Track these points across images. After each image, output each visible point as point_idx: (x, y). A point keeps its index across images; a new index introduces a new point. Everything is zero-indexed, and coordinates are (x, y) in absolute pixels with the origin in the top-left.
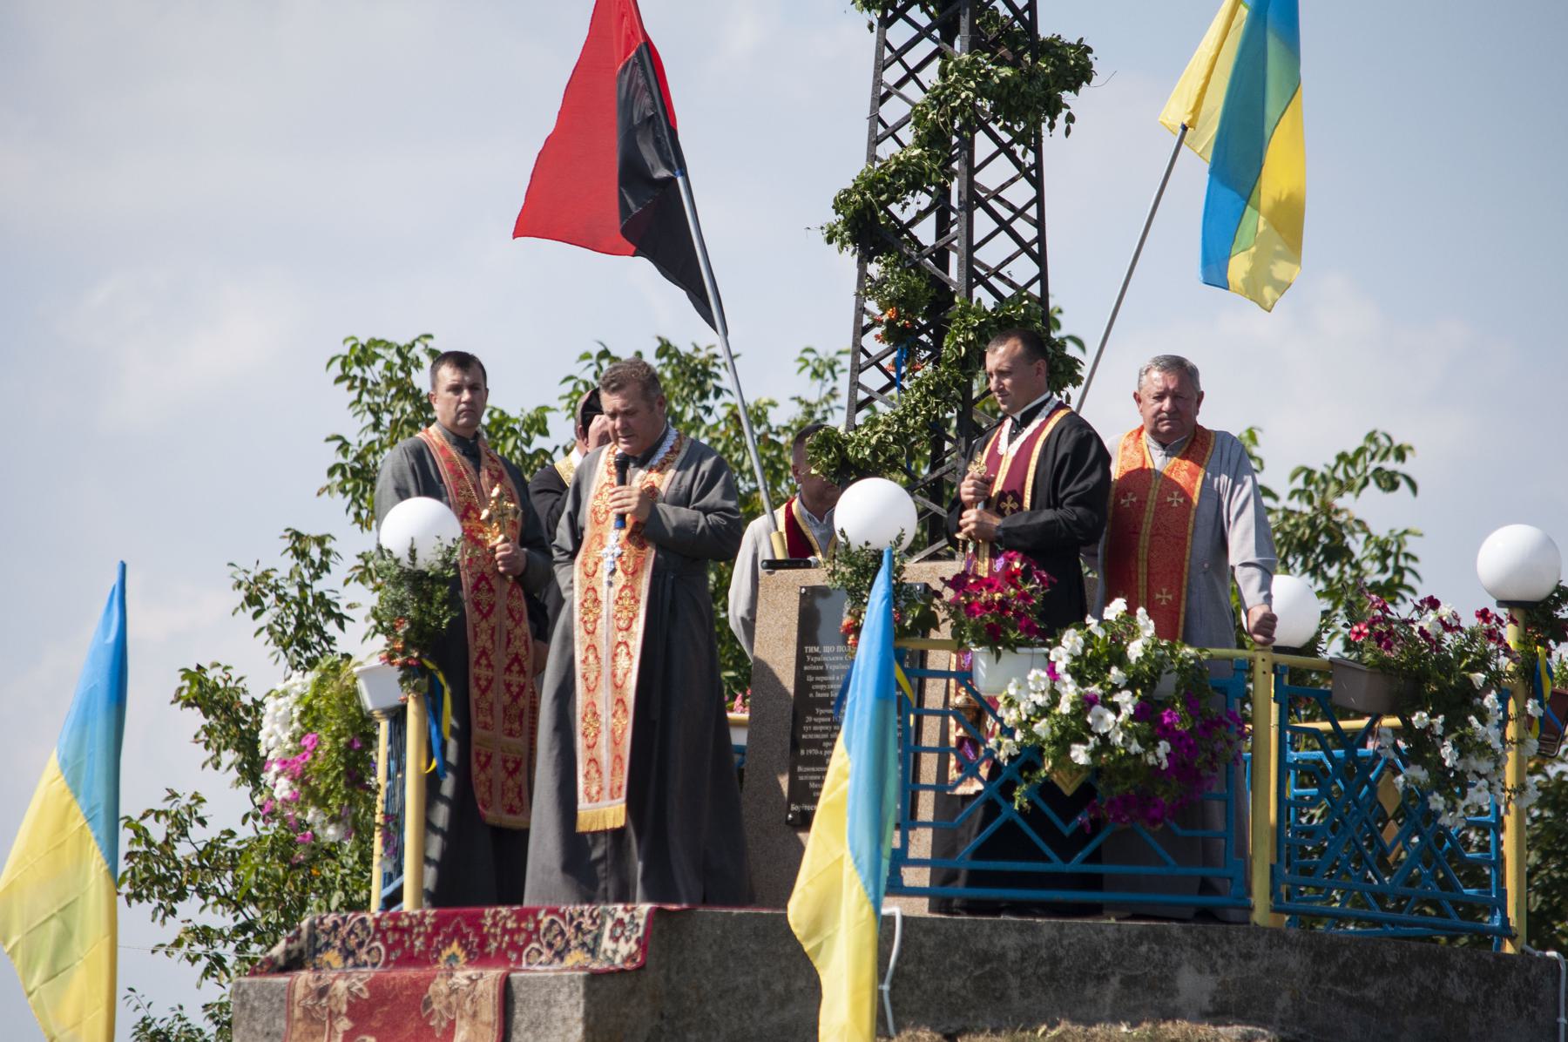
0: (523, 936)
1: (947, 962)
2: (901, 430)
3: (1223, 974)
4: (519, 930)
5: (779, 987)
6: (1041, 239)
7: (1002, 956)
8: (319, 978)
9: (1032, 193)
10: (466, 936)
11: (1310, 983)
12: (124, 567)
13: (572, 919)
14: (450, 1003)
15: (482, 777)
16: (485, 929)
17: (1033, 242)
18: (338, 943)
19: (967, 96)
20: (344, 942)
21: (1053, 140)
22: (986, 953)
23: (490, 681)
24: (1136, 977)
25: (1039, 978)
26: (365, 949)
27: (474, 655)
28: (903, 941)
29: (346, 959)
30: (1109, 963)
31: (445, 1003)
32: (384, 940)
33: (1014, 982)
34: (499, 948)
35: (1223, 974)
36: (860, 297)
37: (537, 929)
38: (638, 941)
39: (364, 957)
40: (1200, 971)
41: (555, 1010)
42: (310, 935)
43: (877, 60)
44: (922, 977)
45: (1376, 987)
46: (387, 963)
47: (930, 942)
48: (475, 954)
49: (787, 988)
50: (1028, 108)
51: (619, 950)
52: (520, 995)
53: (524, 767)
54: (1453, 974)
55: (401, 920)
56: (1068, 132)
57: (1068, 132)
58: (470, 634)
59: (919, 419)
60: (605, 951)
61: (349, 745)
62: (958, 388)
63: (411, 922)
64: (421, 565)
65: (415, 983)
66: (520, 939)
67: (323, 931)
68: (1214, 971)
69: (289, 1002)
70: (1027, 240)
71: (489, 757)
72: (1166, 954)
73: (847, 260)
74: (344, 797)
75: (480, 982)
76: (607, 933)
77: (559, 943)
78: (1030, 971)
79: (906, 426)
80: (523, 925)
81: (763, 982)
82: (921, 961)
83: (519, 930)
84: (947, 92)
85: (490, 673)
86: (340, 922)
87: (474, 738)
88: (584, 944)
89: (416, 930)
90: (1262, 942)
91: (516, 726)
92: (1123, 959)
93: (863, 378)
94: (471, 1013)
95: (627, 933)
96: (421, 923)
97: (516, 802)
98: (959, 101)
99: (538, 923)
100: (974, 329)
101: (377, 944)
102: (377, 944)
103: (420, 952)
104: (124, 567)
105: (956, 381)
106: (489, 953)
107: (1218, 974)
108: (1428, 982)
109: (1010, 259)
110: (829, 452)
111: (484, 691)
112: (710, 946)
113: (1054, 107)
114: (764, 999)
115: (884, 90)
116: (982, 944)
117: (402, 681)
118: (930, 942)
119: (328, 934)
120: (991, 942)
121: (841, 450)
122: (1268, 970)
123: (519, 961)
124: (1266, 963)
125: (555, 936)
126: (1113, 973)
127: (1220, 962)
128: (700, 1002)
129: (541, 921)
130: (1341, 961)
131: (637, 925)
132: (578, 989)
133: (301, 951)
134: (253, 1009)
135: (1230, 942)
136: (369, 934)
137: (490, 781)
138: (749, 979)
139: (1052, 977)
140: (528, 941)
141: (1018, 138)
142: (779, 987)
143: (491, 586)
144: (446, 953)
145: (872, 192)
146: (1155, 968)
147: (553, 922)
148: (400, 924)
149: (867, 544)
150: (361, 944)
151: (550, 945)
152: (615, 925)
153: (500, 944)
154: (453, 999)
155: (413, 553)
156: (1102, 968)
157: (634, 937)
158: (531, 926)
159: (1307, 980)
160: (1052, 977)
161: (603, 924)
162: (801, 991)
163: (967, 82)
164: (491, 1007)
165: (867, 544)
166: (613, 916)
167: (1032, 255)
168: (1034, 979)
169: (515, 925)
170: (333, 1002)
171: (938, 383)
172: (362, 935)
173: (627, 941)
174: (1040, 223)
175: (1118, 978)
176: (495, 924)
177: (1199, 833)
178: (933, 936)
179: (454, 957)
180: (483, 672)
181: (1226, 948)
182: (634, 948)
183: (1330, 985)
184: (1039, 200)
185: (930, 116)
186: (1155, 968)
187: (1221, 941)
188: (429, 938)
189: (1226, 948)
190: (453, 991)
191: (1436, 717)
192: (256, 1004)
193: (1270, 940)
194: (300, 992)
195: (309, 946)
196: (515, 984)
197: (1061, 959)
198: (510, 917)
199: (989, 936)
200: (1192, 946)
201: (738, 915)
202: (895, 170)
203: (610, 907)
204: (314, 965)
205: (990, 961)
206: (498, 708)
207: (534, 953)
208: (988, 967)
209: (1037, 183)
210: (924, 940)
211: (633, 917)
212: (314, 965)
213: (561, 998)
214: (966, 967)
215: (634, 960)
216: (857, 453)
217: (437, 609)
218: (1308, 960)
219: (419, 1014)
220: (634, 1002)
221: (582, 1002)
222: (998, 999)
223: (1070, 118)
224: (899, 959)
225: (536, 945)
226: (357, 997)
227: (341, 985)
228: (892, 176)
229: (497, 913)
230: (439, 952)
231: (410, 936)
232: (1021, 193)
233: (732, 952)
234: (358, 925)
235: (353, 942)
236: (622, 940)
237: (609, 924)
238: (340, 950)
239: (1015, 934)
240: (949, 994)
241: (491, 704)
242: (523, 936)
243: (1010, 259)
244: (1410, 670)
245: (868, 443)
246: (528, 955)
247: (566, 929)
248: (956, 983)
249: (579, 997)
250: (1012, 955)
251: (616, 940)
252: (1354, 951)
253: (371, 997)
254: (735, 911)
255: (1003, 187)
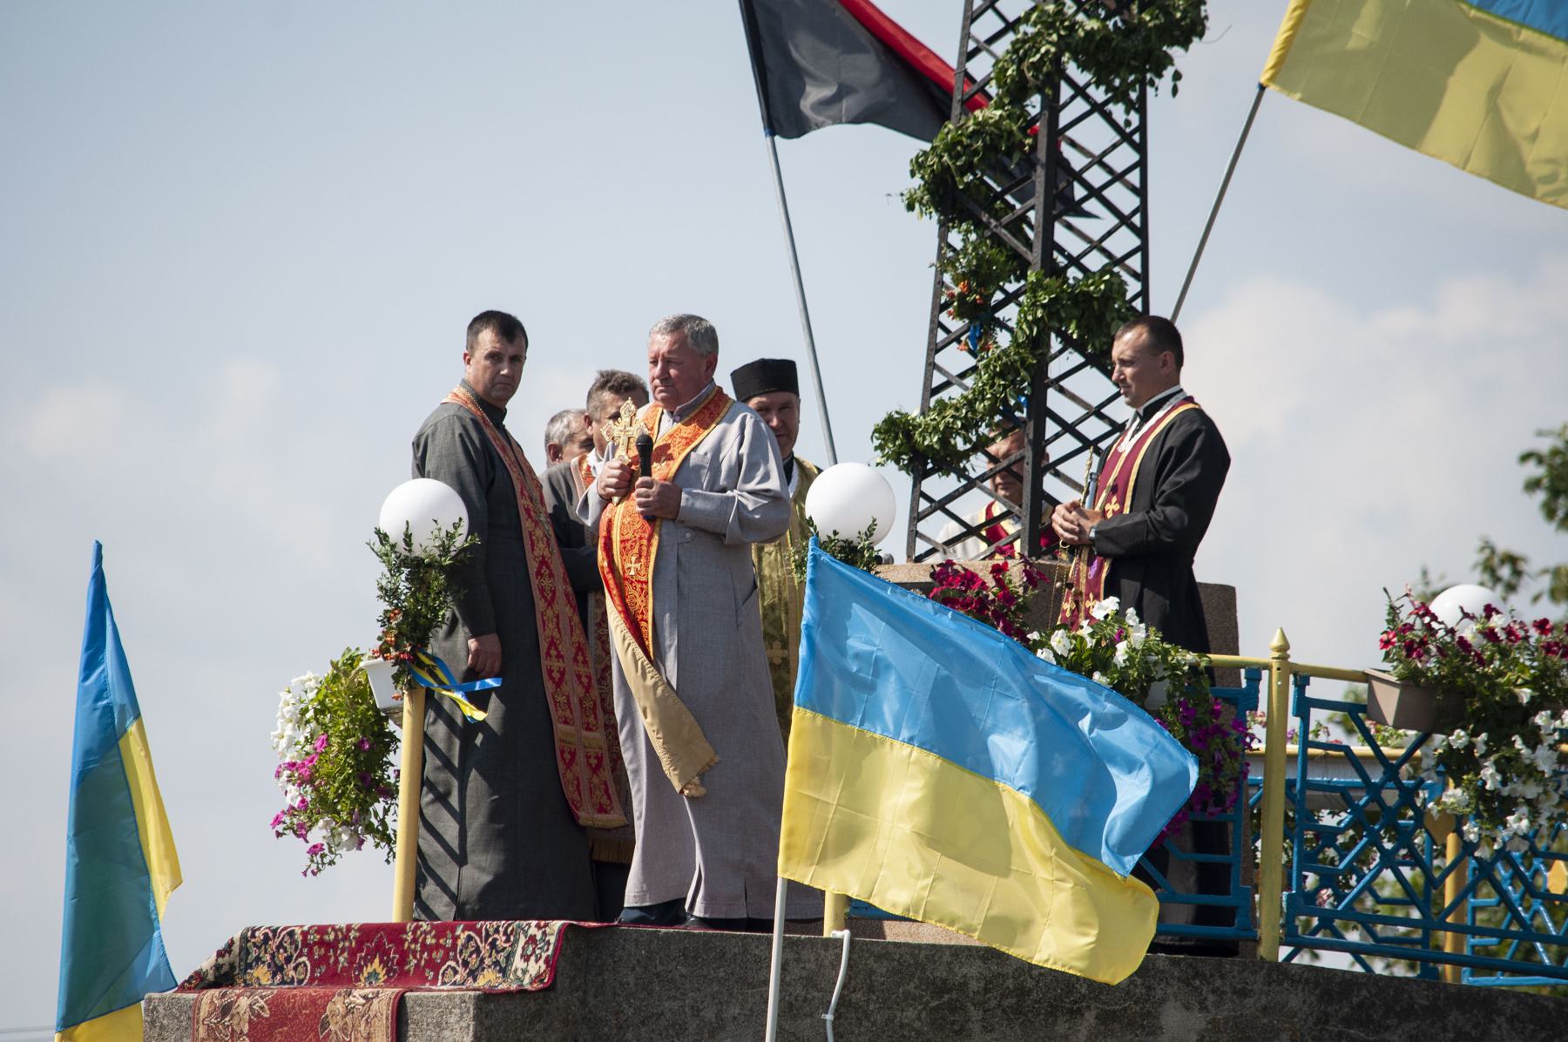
0: (441, 952)
1: (901, 990)
2: (970, 415)
3: (1213, 1012)
4: (438, 946)
5: (709, 1014)
6: (1143, 209)
7: (963, 986)
8: (224, 996)
9: (1134, 157)
10: (387, 952)
11: (1316, 1024)
12: (99, 547)
13: (488, 935)
14: (346, 1023)
15: (569, 775)
16: (406, 945)
17: (1134, 213)
18: (268, 957)
19: (1047, 52)
20: (273, 956)
21: (1158, 99)
22: (944, 981)
23: (562, 673)
24: (1114, 1012)
25: (1004, 1011)
26: (292, 965)
27: (544, 646)
28: (849, 967)
29: (274, 975)
30: (1084, 996)
31: (341, 1024)
32: (310, 955)
33: (975, 1014)
34: (417, 966)
35: (1213, 1012)
36: (941, 271)
37: (454, 945)
38: (547, 961)
39: (292, 973)
40: (1187, 1007)
41: (447, 1033)
42: (241, 948)
43: (966, 11)
44: (871, 1007)
45: (1399, 1031)
46: (312, 980)
47: (881, 969)
48: (395, 972)
49: (719, 1015)
50: (1121, 64)
51: (528, 970)
52: (414, 1015)
53: (606, 762)
54: (1501, 1020)
55: (327, 933)
56: (1175, 91)
57: (1175, 91)
58: (539, 623)
59: (987, 403)
60: (516, 970)
61: (359, 745)
62: (1027, 369)
63: (336, 936)
64: (417, 552)
65: (313, 1001)
66: (438, 956)
67: (254, 944)
68: (1203, 1008)
69: (193, 1020)
70: (1127, 212)
71: (573, 754)
72: (1149, 988)
73: (927, 224)
74: (354, 802)
75: (375, 1001)
76: (519, 951)
77: (474, 961)
78: (993, 1003)
79: (974, 411)
80: (441, 941)
81: (693, 1008)
82: (871, 989)
83: (438, 946)
84: (1027, 46)
85: (561, 664)
86: (271, 935)
87: (558, 735)
88: (496, 963)
89: (340, 946)
90: (1260, 978)
91: (591, 719)
92: (1101, 992)
93: (940, 359)
94: (365, 1035)
95: (538, 952)
96: (346, 938)
97: (604, 800)
98: (1038, 56)
99: (455, 938)
100: (1044, 306)
101: (304, 959)
102: (304, 959)
103: (343, 967)
104: (99, 547)
105: (1023, 361)
106: (409, 971)
107: (1208, 1012)
108: (1468, 1028)
109: (1110, 233)
110: (896, 438)
111: (558, 684)
112: (633, 969)
113: (1161, 63)
114: (692, 1026)
115: (972, 45)
116: (941, 973)
117: (396, 678)
118: (881, 969)
119: (259, 948)
120: (951, 970)
121: (909, 436)
122: (1265, 1008)
123: (435, 981)
124: (1264, 1001)
125: (470, 956)
126: (1088, 1007)
127: (1211, 998)
128: (620, 1028)
129: (459, 937)
130: (1355, 1000)
131: (548, 943)
132: (468, 1012)
133: (232, 966)
134: (162, 1027)
135: (1222, 977)
136: (296, 950)
137: (578, 779)
138: (675, 1005)
139: (1018, 1010)
140: (445, 959)
141: (1119, 95)
142: (709, 1014)
143: (550, 571)
144: (368, 970)
145: (950, 155)
146: (1136, 1003)
147: (470, 938)
148: (326, 937)
149: (835, 533)
150: (288, 960)
151: (465, 964)
152: (527, 943)
153: (419, 961)
154: (348, 1019)
155: (408, 538)
156: (1075, 1002)
157: (544, 955)
158: (449, 942)
159: (1311, 1020)
160: (1018, 1010)
161: (517, 941)
162: (735, 1018)
163: (1050, 35)
164: (383, 1028)
165: (835, 533)
166: (525, 933)
167: (1132, 227)
168: (999, 1012)
169: (434, 941)
170: (235, 1022)
171: (1006, 364)
172: (290, 949)
173: (537, 961)
174: (1141, 191)
175: (1094, 1013)
176: (415, 941)
177: (1218, 858)
178: (885, 963)
179: (375, 974)
180: (556, 664)
181: (1218, 983)
182: (543, 967)
183: (1340, 1027)
184: (1142, 164)
185: (1009, 72)
186: (1136, 1003)
187: (1212, 976)
188: (353, 953)
189: (1218, 983)
190: (349, 1011)
191: (1478, 735)
192: (165, 1022)
193: (1269, 975)
194: (205, 1009)
195: (241, 960)
196: (409, 1004)
197: (1030, 991)
198: (430, 932)
199: (949, 964)
200: (1179, 979)
201: (666, 933)
202: (974, 130)
203: (524, 923)
204: (245, 981)
205: (949, 991)
206: (575, 700)
207: (450, 971)
208: (946, 997)
209: (1141, 148)
210: (875, 965)
211: (544, 934)
212: (245, 981)
213: (452, 1020)
214: (922, 996)
215: (542, 981)
216: (924, 439)
217: (434, 600)
218: (1313, 998)
219: (316, 1035)
220: (540, 1026)
221: (472, 1023)
222: (957, 1033)
223: (1177, 76)
224: (844, 986)
225: (452, 963)
226: (259, 1016)
227: (244, 1002)
228: (970, 136)
229: (418, 927)
230: (361, 971)
231: (335, 952)
232: (1123, 157)
233: (658, 975)
234: (286, 938)
235: (281, 956)
236: (533, 959)
237: (522, 941)
238: (269, 966)
239: (979, 962)
240: (902, 1026)
241: (568, 697)
242: (441, 952)
243: (1110, 233)
244: (1452, 683)
245: (936, 429)
246: (443, 974)
247: (481, 946)
248: (911, 1013)
249: (469, 1020)
250: (974, 985)
251: (526, 958)
252: (1374, 992)
253: (271, 1015)
254: (663, 930)
255: (1105, 153)
